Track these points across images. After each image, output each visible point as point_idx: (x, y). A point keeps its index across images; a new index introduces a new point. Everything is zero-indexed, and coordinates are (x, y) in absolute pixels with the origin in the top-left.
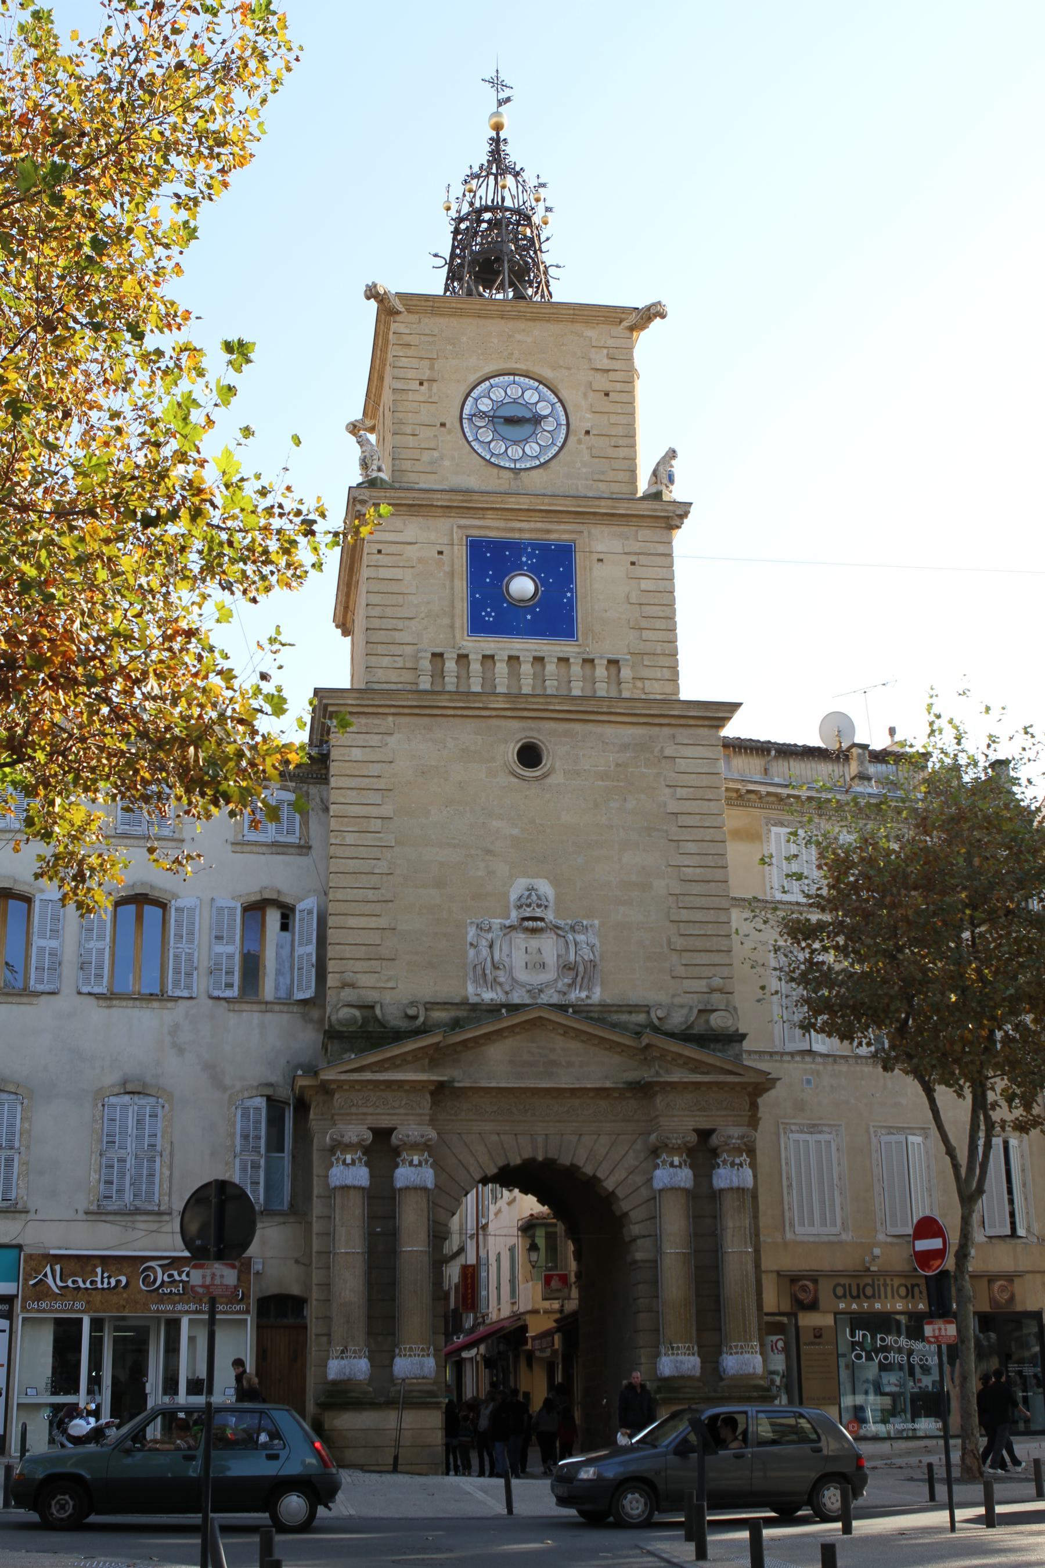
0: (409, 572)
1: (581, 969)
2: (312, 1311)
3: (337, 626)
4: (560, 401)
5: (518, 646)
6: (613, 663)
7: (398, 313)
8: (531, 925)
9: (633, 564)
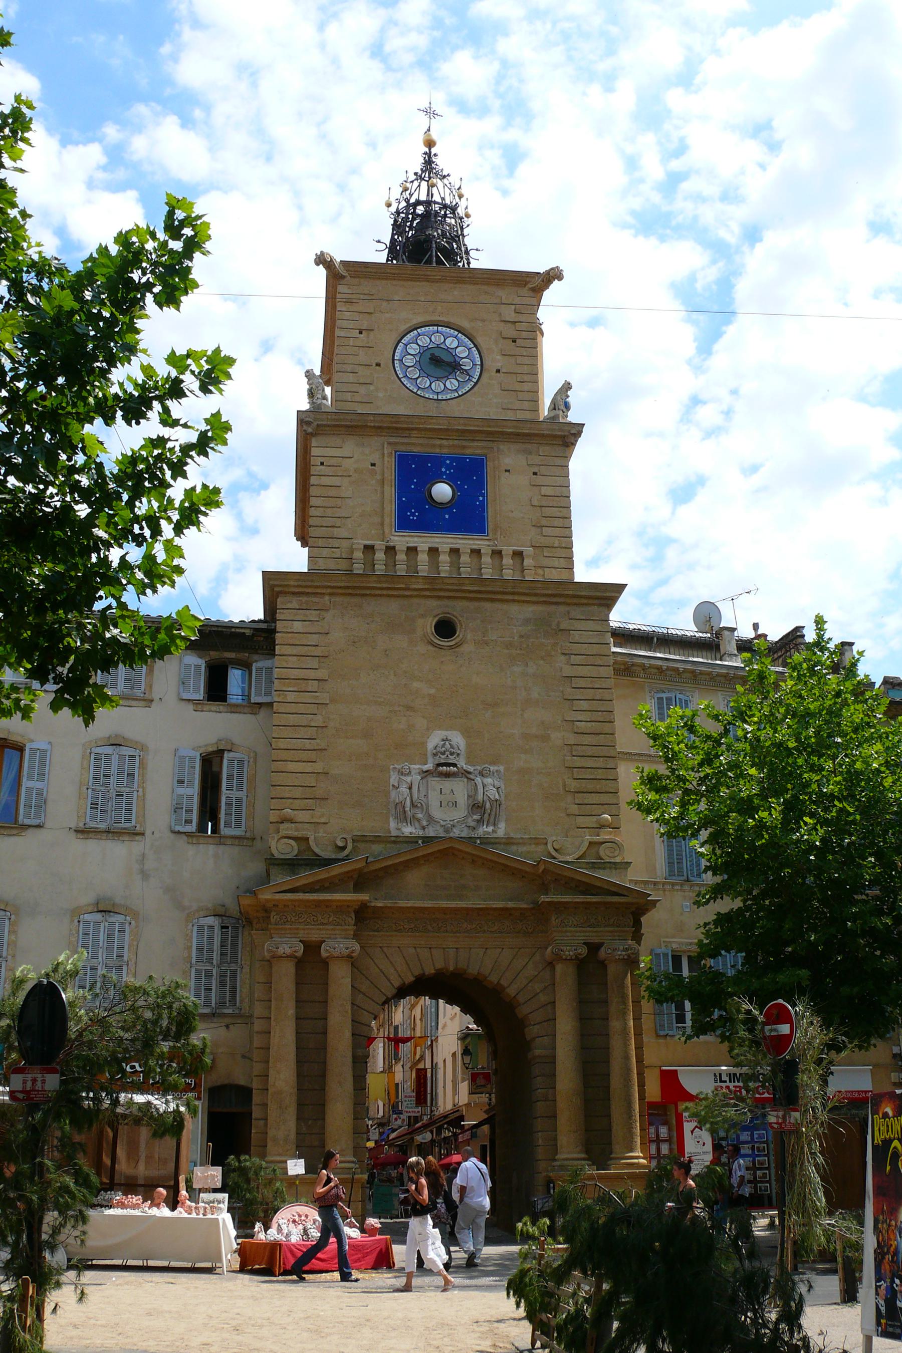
0: (346, 480)
1: (488, 805)
2: (256, 1098)
3: (297, 540)
4: (476, 346)
5: (437, 540)
6: (518, 555)
7: (343, 277)
8: (445, 770)
9: (535, 474)
